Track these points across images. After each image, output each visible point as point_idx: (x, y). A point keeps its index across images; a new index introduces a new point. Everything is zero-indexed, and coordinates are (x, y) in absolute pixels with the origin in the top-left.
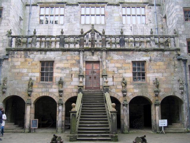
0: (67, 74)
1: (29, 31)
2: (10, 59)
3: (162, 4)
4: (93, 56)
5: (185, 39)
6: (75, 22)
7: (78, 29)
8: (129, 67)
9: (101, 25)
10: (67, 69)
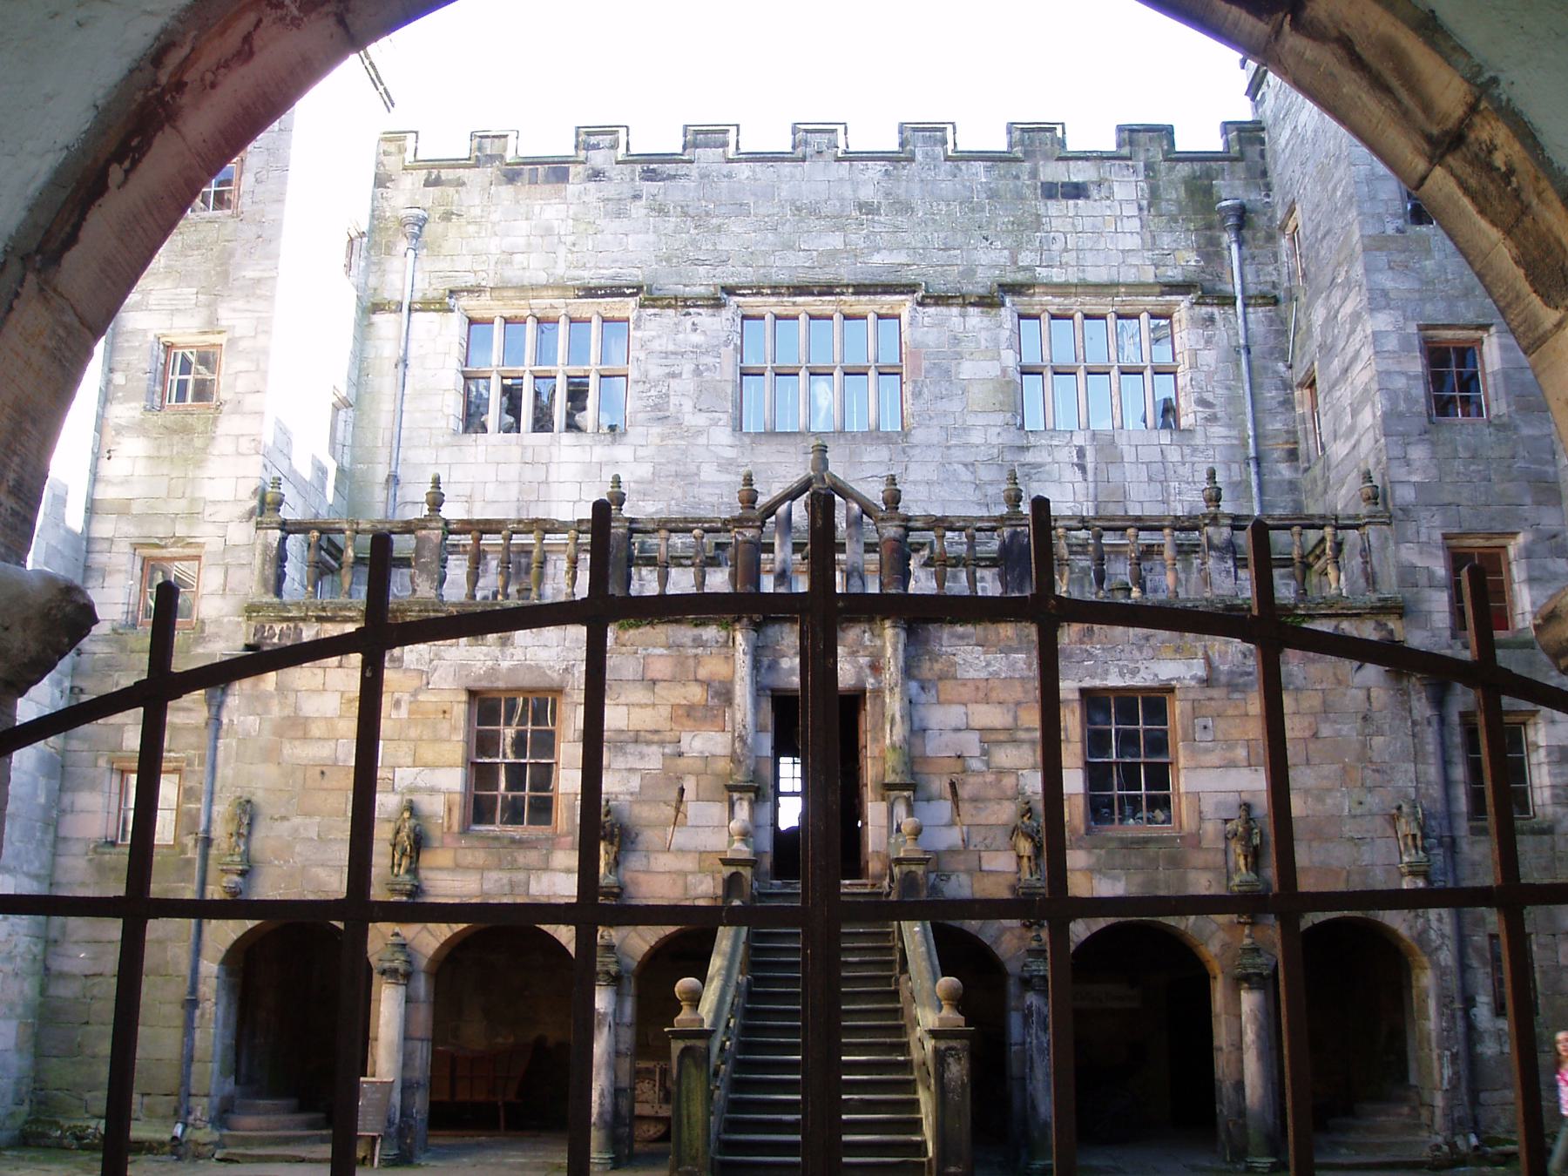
0: (645, 775)
1: (393, 480)
3: (1290, 289)
6: (701, 420)
7: (725, 465)
9: (876, 436)
10: (649, 743)
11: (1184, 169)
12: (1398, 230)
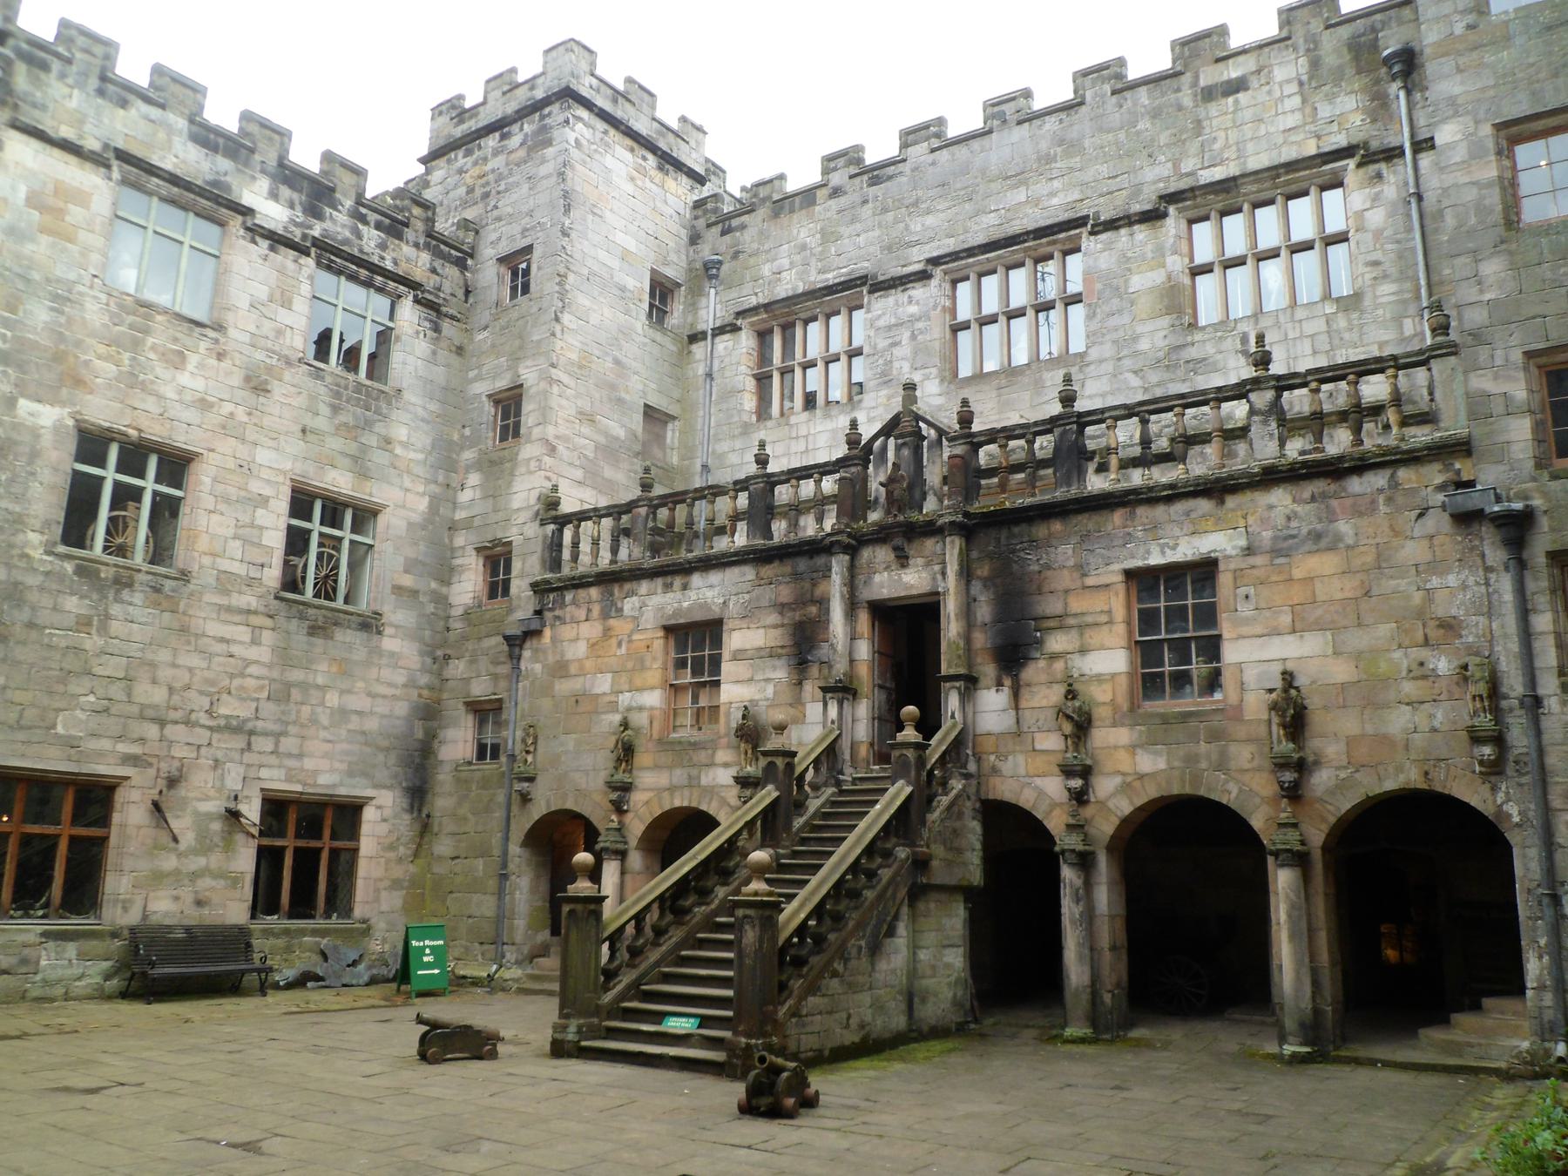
2: (547, 632)
4: (904, 566)
5: (1517, 356)
8: (1109, 612)
11: (1345, 32)
12: (1470, 27)
